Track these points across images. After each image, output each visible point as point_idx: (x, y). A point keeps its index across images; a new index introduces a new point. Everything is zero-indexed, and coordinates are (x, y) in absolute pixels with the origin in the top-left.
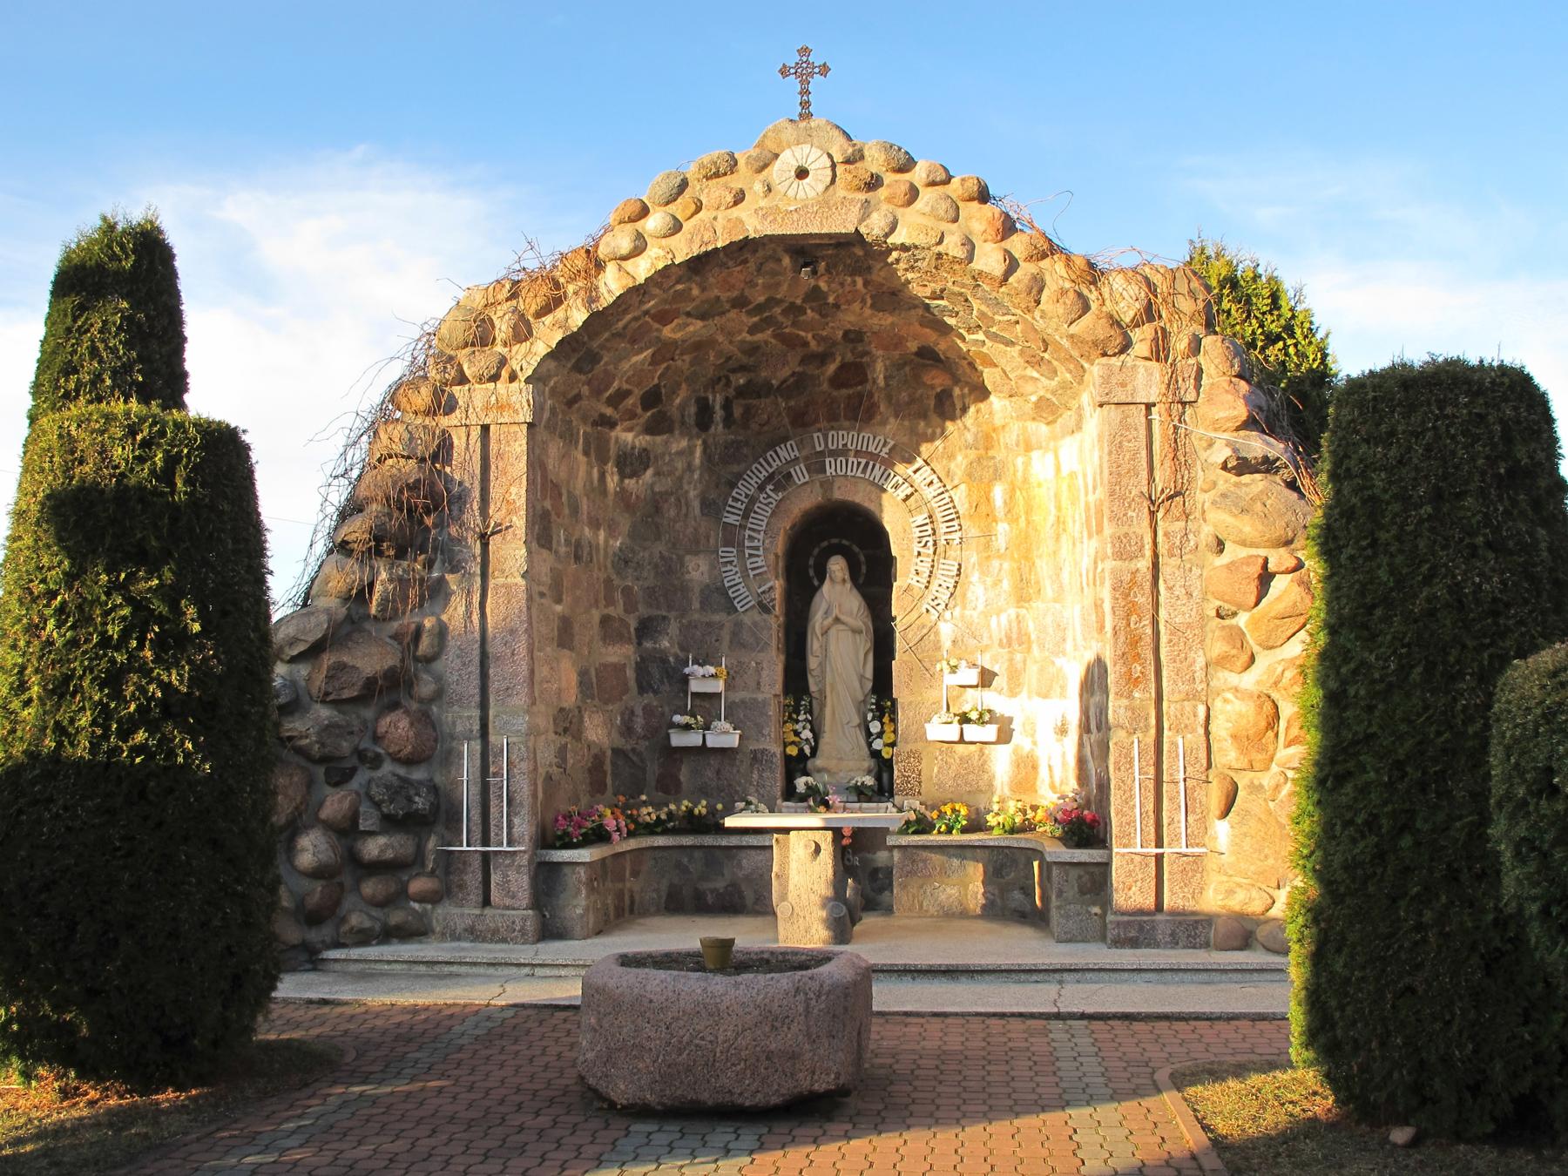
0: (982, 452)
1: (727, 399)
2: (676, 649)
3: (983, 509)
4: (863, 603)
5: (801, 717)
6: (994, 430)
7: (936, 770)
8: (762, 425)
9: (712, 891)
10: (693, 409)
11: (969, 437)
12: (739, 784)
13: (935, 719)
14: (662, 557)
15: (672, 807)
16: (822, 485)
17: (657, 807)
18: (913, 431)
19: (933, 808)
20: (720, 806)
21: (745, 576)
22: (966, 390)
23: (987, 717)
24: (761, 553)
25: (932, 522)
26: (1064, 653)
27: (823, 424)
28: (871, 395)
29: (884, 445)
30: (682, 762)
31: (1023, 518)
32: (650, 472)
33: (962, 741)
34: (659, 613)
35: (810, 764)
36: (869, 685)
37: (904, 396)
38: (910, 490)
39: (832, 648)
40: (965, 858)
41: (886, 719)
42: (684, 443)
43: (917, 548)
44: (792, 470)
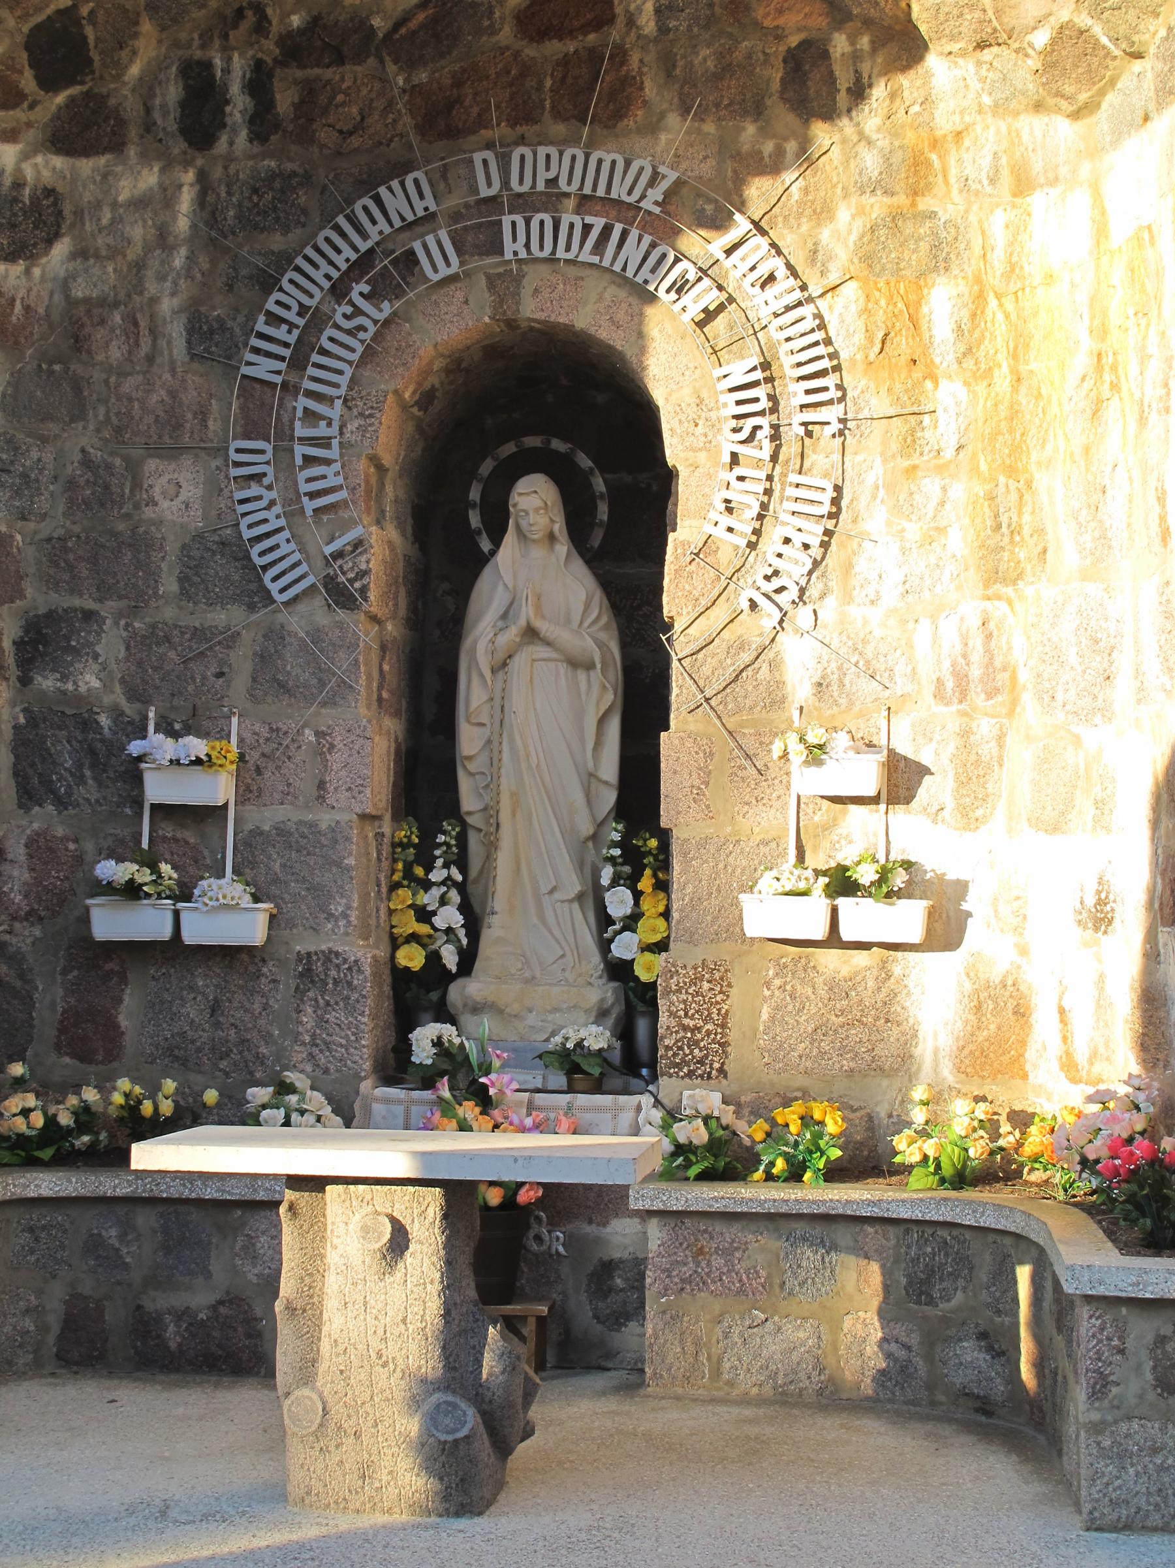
0: (902, 200)
1: (258, 65)
2: (118, 697)
3: (902, 346)
4: (598, 595)
5: (437, 875)
6: (935, 144)
7: (765, 1016)
8: (345, 134)
9: (181, 1315)
10: (172, 92)
11: (871, 161)
12: (267, 1038)
13: (766, 882)
14: (87, 462)
15: (90, 1095)
16: (492, 281)
17: (50, 1090)
18: (726, 149)
19: (758, 1110)
20: (211, 1096)
21: (294, 513)
22: (865, 42)
23: (899, 880)
24: (334, 453)
25: (770, 380)
26: (1106, 712)
27: (499, 131)
28: (620, 55)
29: (652, 183)
30: (123, 980)
31: (1005, 369)
32: (61, 249)
33: (833, 940)
34: (77, 602)
35: (455, 992)
36: (609, 798)
37: (705, 58)
38: (712, 298)
39: (518, 702)
40: (834, 1247)
41: (646, 883)
42: (150, 178)
43: (728, 444)
44: (417, 246)
